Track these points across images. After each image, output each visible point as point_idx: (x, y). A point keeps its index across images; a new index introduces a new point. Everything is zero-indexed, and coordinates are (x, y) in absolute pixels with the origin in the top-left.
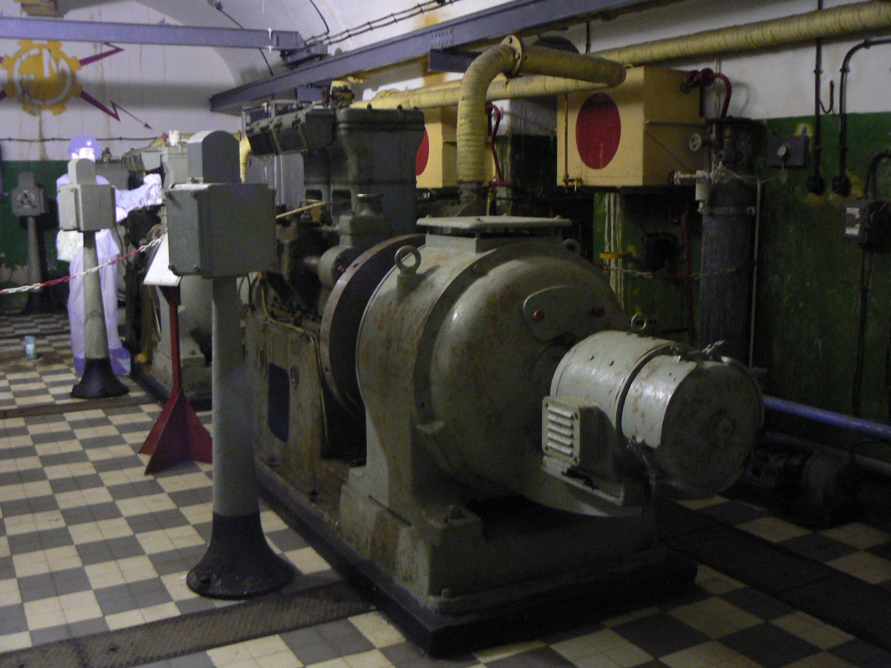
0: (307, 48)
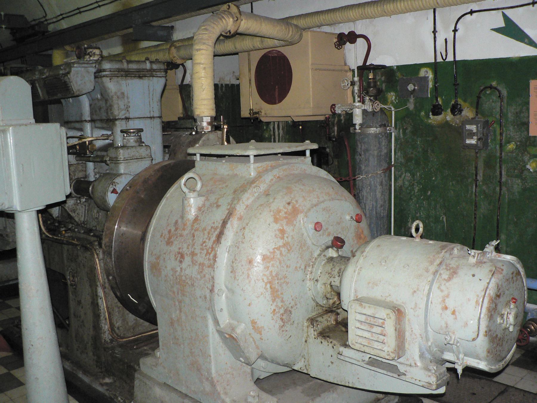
0: (33, 27)
